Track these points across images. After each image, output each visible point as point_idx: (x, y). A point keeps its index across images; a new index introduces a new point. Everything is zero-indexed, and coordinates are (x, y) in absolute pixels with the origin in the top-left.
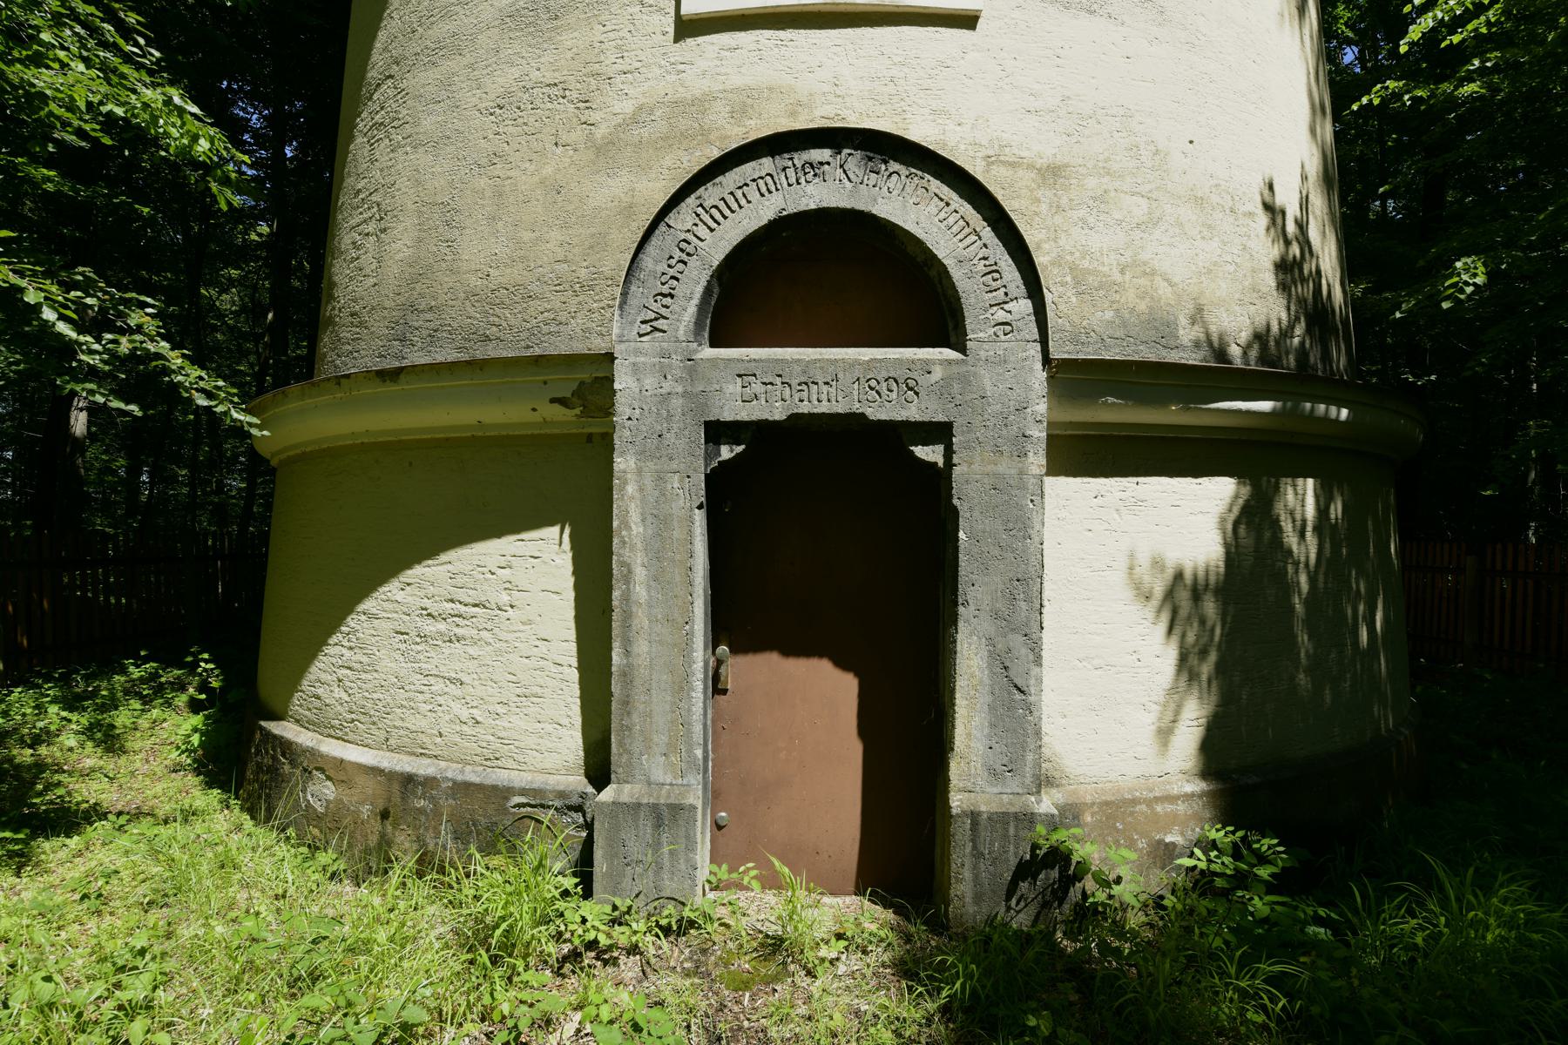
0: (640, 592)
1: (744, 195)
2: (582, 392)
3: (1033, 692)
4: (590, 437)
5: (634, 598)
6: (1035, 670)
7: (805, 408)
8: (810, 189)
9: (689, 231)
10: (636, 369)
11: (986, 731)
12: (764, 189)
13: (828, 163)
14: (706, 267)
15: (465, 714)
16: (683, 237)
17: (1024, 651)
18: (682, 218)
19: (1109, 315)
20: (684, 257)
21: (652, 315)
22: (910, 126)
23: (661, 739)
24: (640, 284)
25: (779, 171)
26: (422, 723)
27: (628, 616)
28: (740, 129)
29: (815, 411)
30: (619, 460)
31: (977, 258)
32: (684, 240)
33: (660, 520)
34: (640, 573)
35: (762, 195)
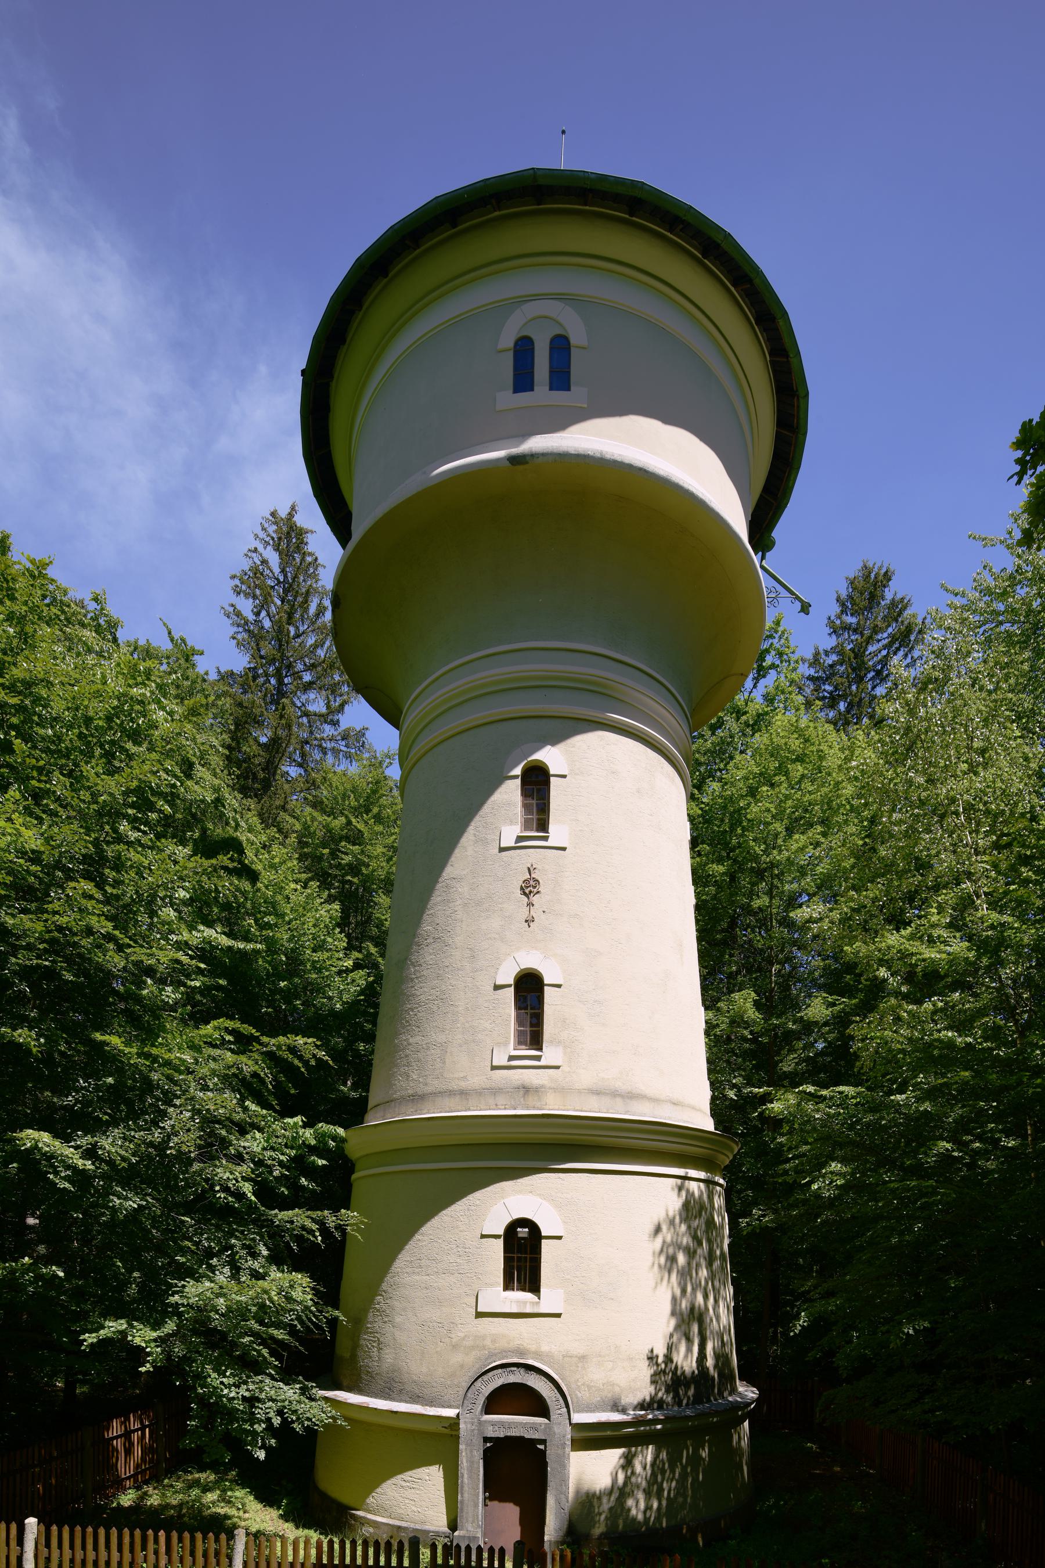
0: (466, 1480)
2: (450, 1425)
4: (452, 1435)
7: (509, 1434)
10: (465, 1422)
15: (416, 1509)
18: (478, 1384)
19: (599, 1399)
23: (470, 1519)
26: (403, 1512)
27: (462, 1487)
33: (471, 1462)
34: (466, 1476)
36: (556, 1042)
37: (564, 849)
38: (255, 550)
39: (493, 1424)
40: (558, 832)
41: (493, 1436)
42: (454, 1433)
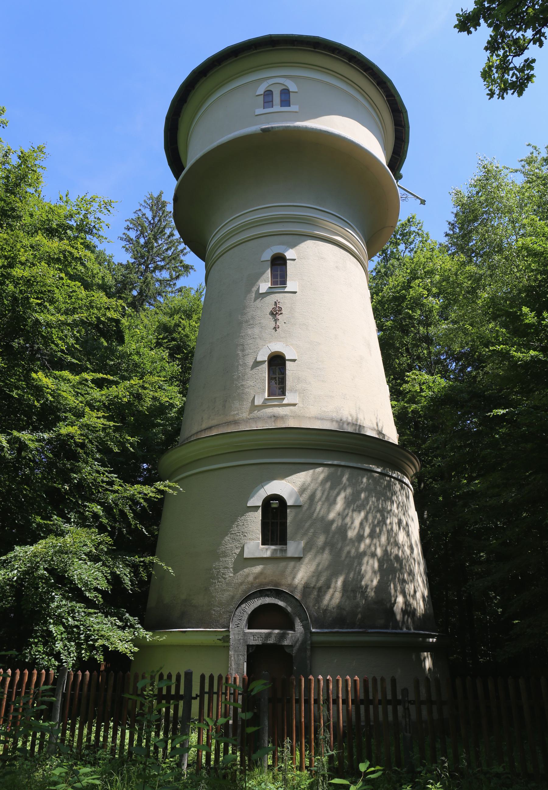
4: (224, 646)
36: (294, 391)
37: (295, 293)
38: (140, 210)
39: (254, 635)
40: (290, 286)
41: (254, 644)
42: (226, 644)
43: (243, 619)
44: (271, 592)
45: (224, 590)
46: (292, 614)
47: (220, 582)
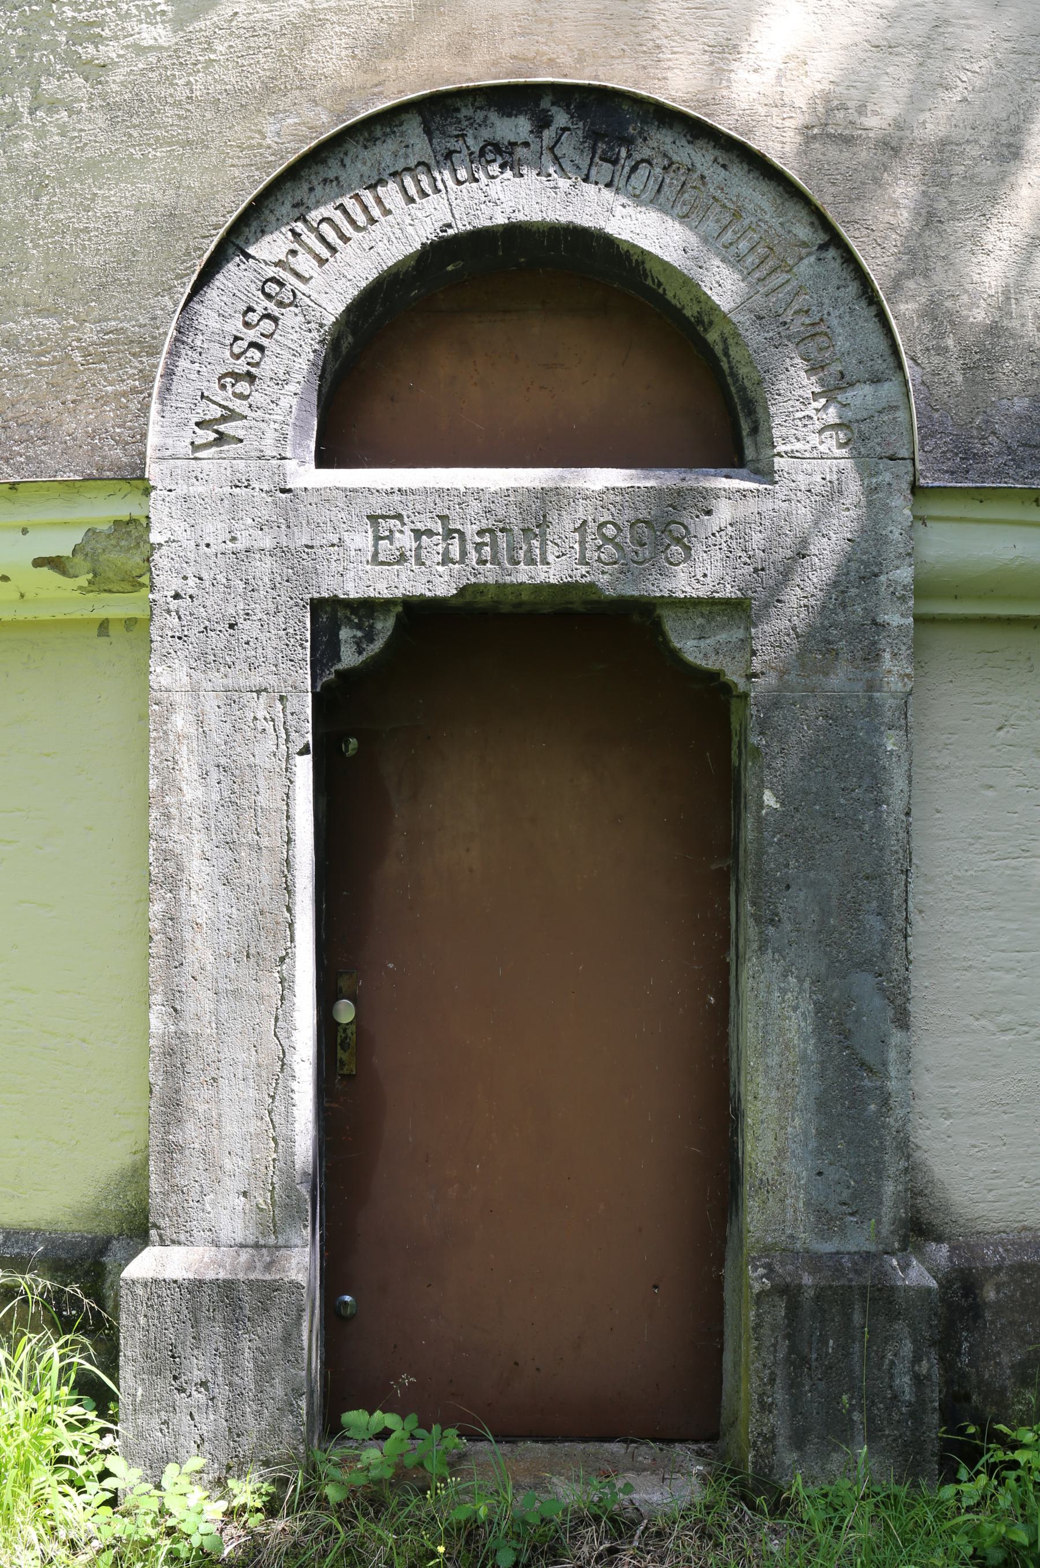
1: (379, 201)
3: (893, 1074)
4: (104, 627)
5: (185, 916)
6: (897, 1037)
8: (495, 189)
9: (279, 264)
11: (813, 1144)
12: (412, 191)
13: (526, 144)
14: (313, 326)
16: (271, 274)
17: (878, 1001)
20: (273, 309)
21: (216, 412)
22: (669, 74)
24: (196, 356)
25: (440, 158)
28: (368, 76)
29: (508, 579)
30: (159, 669)
31: (790, 312)
32: (272, 279)
35: (412, 200)
43: (268, 367)
44: (542, 123)
45: (92, 165)
46: (742, 320)
47: (52, 107)
